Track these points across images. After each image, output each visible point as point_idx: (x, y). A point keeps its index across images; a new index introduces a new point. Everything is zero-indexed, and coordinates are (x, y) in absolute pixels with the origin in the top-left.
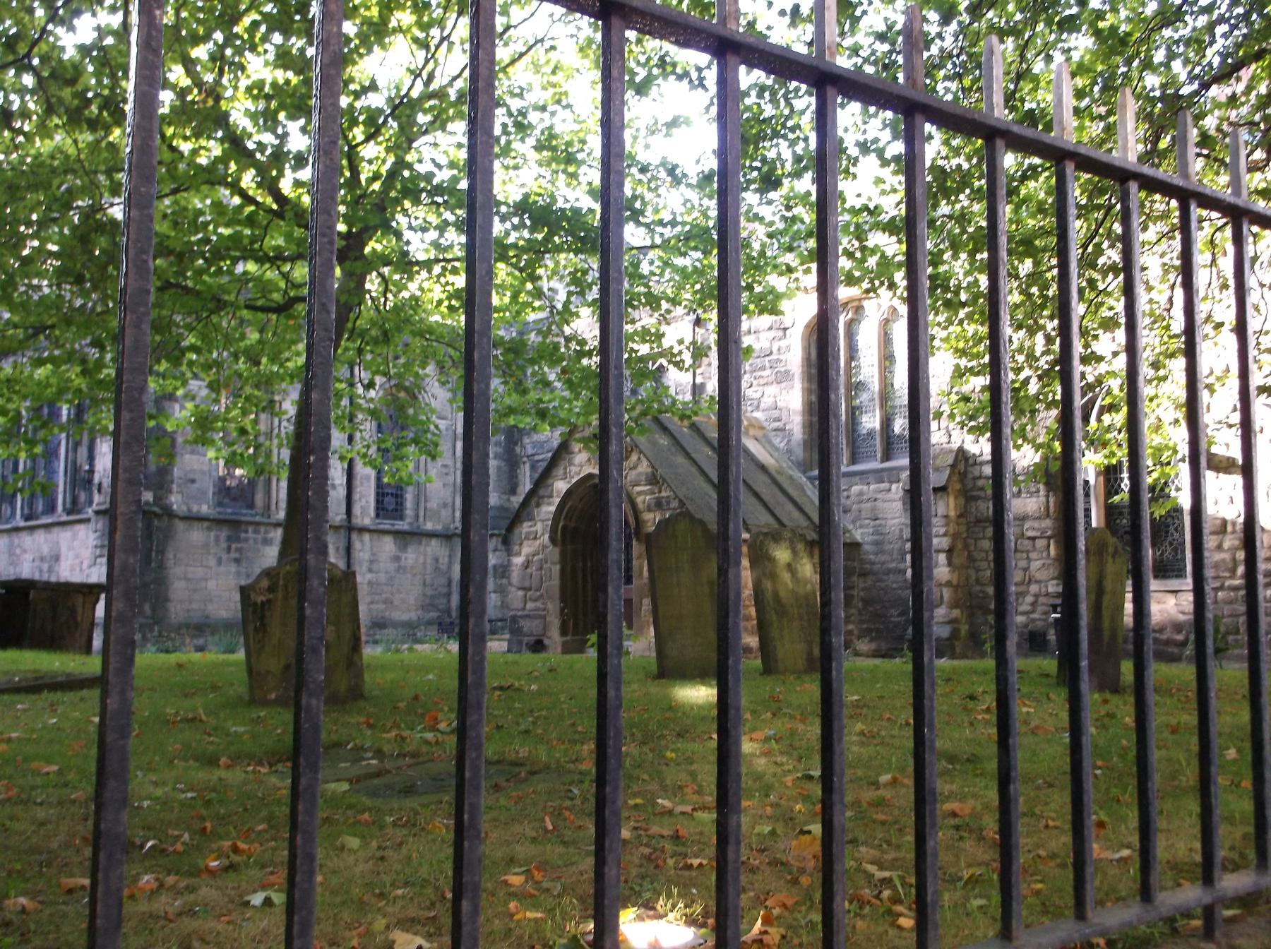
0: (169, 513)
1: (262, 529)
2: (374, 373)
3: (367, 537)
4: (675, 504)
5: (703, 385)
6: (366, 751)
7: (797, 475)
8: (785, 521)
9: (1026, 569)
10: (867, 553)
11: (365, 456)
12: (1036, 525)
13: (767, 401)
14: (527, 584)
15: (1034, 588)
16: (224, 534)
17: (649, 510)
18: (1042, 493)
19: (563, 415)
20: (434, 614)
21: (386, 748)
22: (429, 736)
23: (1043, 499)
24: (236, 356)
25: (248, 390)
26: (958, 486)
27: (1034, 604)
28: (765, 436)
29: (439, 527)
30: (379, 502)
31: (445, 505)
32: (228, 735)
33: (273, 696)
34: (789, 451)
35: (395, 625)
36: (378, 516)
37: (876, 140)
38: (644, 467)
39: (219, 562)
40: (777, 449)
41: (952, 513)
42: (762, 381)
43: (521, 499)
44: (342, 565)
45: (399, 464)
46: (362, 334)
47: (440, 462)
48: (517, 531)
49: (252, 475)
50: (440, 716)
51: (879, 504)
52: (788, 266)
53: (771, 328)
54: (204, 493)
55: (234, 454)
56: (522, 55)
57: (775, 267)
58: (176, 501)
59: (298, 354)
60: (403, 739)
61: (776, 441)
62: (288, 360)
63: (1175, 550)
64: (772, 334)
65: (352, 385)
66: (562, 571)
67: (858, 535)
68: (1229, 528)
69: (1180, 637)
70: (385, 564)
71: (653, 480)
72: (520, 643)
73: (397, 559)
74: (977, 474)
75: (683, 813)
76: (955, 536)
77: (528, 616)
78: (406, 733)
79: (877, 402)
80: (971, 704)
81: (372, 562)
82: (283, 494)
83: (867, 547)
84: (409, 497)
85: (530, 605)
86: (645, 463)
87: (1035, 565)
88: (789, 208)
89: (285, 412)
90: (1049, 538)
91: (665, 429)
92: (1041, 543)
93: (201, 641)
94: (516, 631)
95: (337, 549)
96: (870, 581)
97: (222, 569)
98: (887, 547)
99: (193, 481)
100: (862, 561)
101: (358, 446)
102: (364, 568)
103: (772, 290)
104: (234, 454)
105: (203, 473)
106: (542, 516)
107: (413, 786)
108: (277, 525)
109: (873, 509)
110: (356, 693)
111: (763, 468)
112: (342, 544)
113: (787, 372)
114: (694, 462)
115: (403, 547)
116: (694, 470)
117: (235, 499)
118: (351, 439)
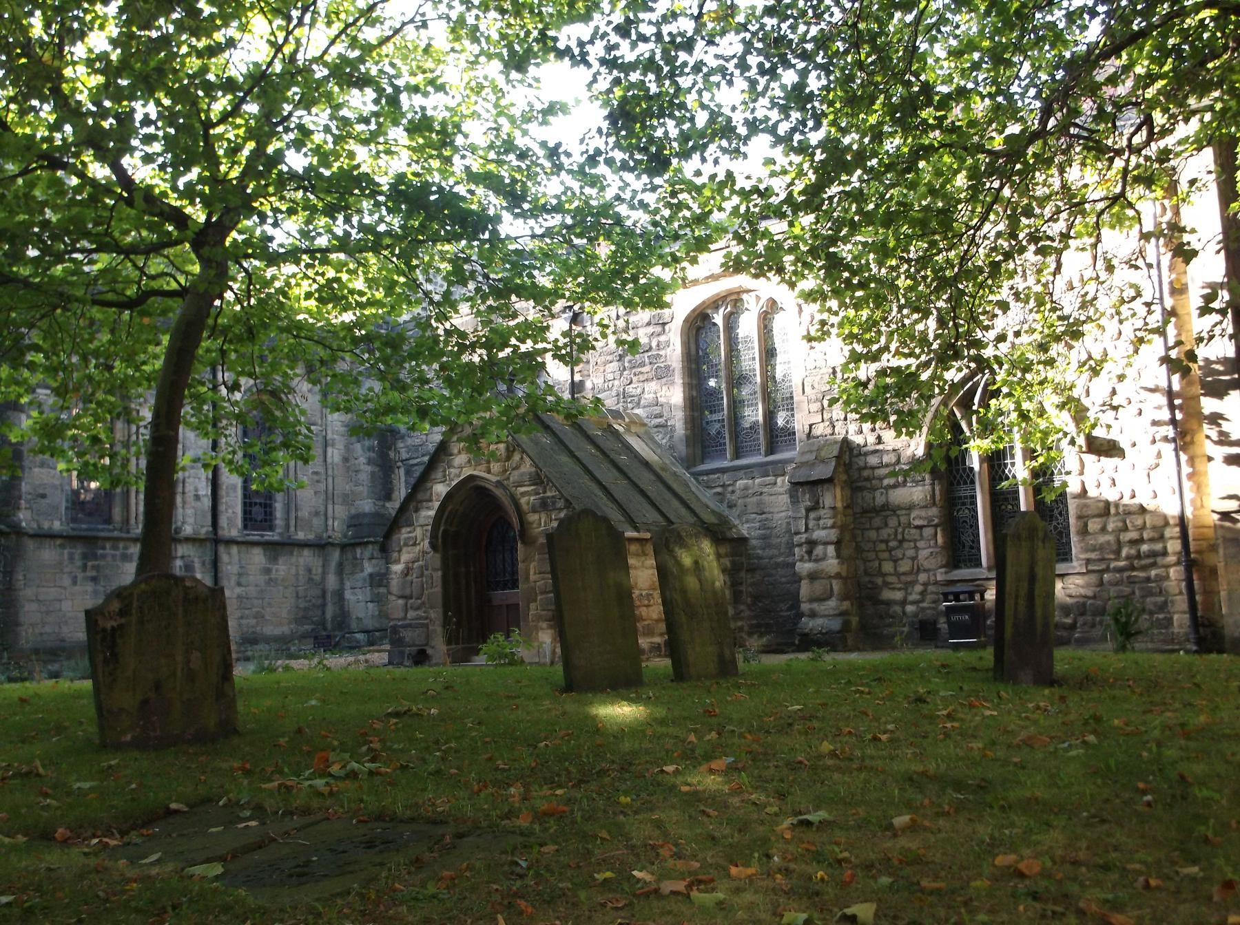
0: (18, 532)
1: (121, 545)
2: (239, 374)
3: (234, 549)
4: (560, 504)
5: (582, 383)
6: (242, 807)
7: (680, 470)
8: (672, 518)
9: (913, 559)
10: (754, 548)
11: (231, 462)
12: (923, 513)
13: (648, 397)
14: (408, 592)
15: (922, 577)
16: (78, 551)
17: (534, 511)
18: (928, 481)
19: (443, 412)
20: (308, 627)
21: (269, 804)
22: (319, 783)
23: (928, 488)
24: (85, 358)
25: (100, 396)
26: (844, 477)
27: (923, 593)
28: (647, 433)
29: (311, 537)
30: (246, 512)
31: (317, 514)
32: (69, 794)
33: (128, 737)
34: (672, 448)
35: (267, 640)
36: (245, 527)
37: (767, 119)
38: (527, 467)
39: (75, 583)
40: (660, 446)
41: (839, 505)
42: (642, 378)
43: (397, 505)
44: (208, 581)
45: (267, 469)
46: (225, 331)
47: (311, 468)
48: (395, 537)
49: (107, 486)
50: (332, 756)
51: (765, 498)
52: (673, 255)
53: (649, 324)
54: (57, 508)
55: (86, 464)
56: (388, 39)
57: (661, 256)
58: (24, 518)
59: (156, 357)
60: (289, 789)
61: (658, 438)
62: (144, 363)
63: (1060, 533)
64: (650, 329)
65: (215, 388)
66: (444, 577)
67: (744, 530)
68: (1113, 511)
69: (1068, 621)
70: (255, 577)
71: (538, 480)
72: (402, 653)
73: (267, 571)
74: (862, 464)
75: (673, 893)
76: (843, 528)
77: (410, 625)
78: (292, 781)
79: (759, 395)
80: (925, 709)
81: (240, 575)
82: (141, 508)
83: (754, 542)
84: (279, 507)
85: (411, 614)
86: (528, 462)
87: (923, 554)
88: (674, 194)
89: (143, 419)
90: (936, 526)
91: (547, 428)
92: (928, 532)
93: (55, 667)
94: (397, 642)
95: (203, 564)
96: (758, 576)
97: (77, 588)
98: (775, 541)
99: (43, 496)
100: (749, 557)
101: (224, 453)
102: (233, 582)
103: (658, 281)
104: (86, 464)
105: (54, 487)
106: (422, 521)
107: (308, 863)
108: (135, 540)
109: (759, 504)
110: (228, 728)
111: (646, 464)
112: (208, 558)
113: (667, 367)
114: (578, 460)
115: (274, 559)
116: (578, 469)
117: (90, 514)
118: (215, 446)
